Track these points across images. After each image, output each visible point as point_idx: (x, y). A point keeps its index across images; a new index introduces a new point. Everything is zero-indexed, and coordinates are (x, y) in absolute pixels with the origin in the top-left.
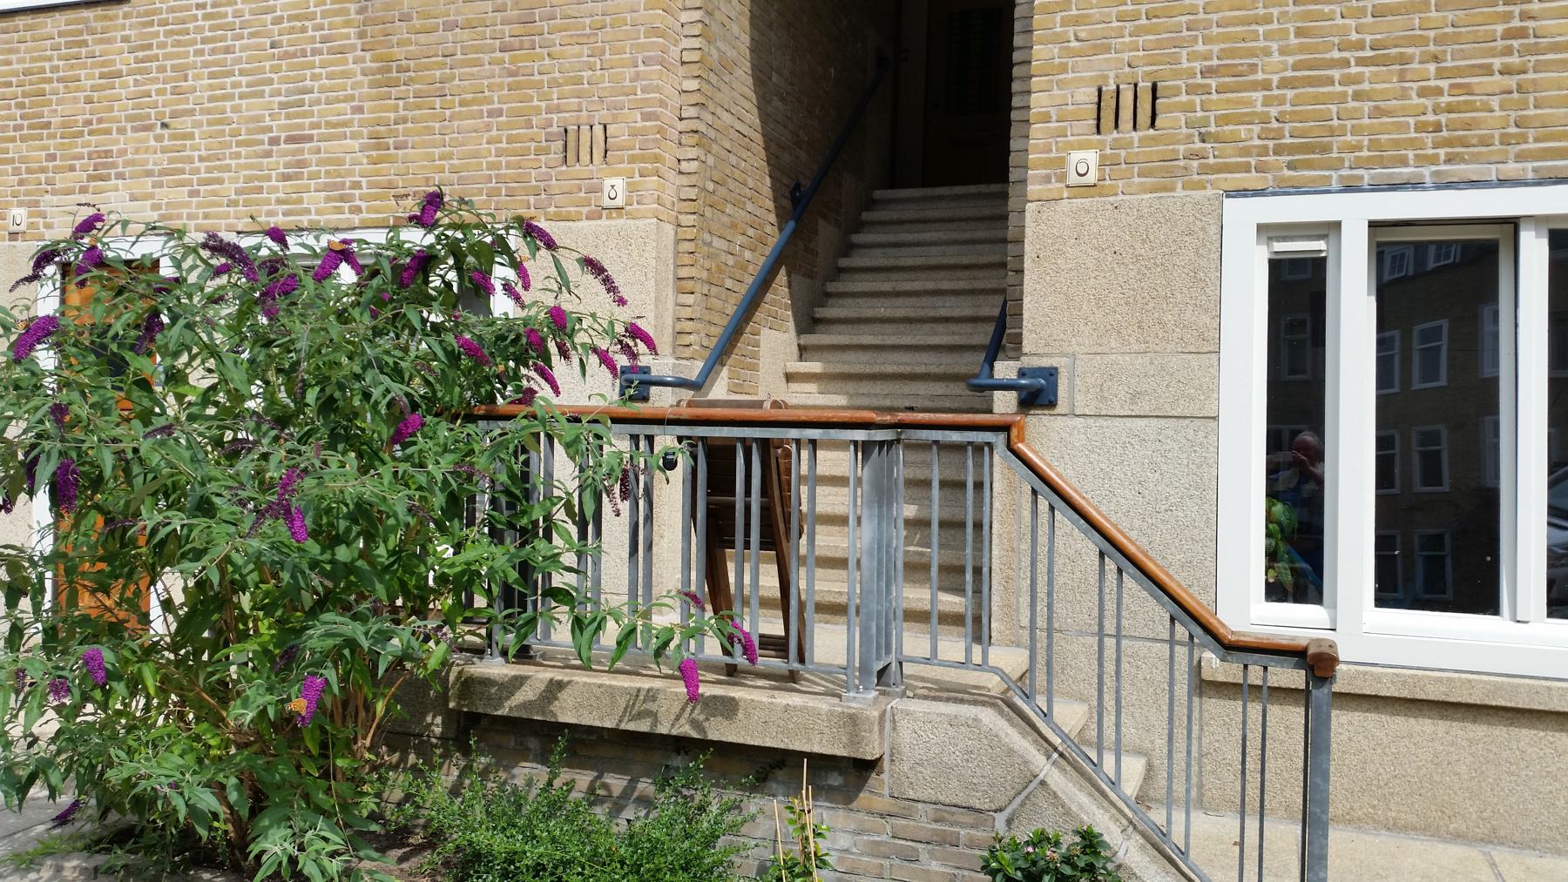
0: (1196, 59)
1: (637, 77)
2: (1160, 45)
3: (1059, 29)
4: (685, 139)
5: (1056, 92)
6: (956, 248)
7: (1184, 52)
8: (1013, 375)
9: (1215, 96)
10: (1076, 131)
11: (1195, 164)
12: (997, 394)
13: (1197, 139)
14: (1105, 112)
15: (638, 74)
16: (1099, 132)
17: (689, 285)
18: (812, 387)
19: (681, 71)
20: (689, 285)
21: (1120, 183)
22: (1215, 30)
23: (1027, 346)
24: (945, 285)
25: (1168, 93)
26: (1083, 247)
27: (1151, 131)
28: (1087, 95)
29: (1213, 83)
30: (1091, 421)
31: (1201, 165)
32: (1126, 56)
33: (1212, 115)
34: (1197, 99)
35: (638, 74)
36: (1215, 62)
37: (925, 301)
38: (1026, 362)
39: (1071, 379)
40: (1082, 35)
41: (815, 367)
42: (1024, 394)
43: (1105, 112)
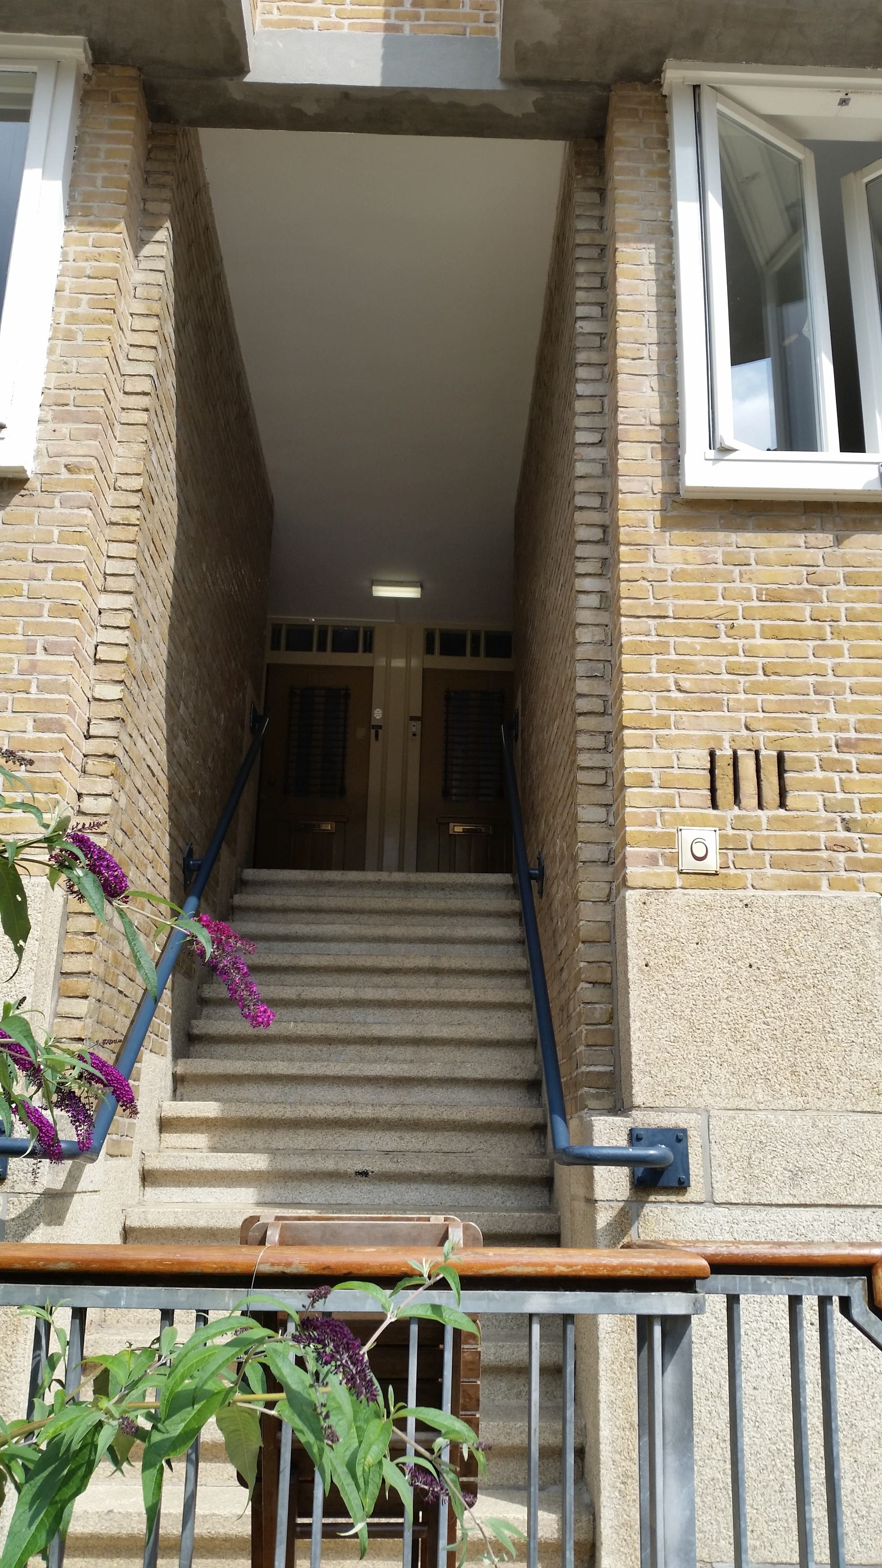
0: (830, 729)
1: (33, 667)
2: (782, 707)
3: (655, 675)
4: (92, 765)
5: (656, 750)
6: (364, 945)
7: (814, 719)
8: (621, 1140)
9: (856, 776)
10: (685, 802)
11: (841, 857)
12: (599, 1171)
13: (839, 826)
14: (721, 781)
15: (34, 665)
16: (714, 806)
17: (82, 984)
18: (200, 1140)
19: (95, 671)
20: (82, 984)
21: (749, 873)
22: (849, 697)
23: (640, 1093)
24: (370, 994)
25: (799, 766)
26: (708, 956)
27: (782, 812)
28: (699, 758)
29: (852, 759)
30: (737, 1212)
31: (848, 859)
32: (742, 716)
33: (855, 798)
34: (836, 777)
35: (34, 665)
36: (853, 735)
37: (340, 1013)
38: (641, 1119)
39: (707, 1145)
40: (686, 685)
41: (209, 1109)
42: (640, 1171)
43: (721, 781)
